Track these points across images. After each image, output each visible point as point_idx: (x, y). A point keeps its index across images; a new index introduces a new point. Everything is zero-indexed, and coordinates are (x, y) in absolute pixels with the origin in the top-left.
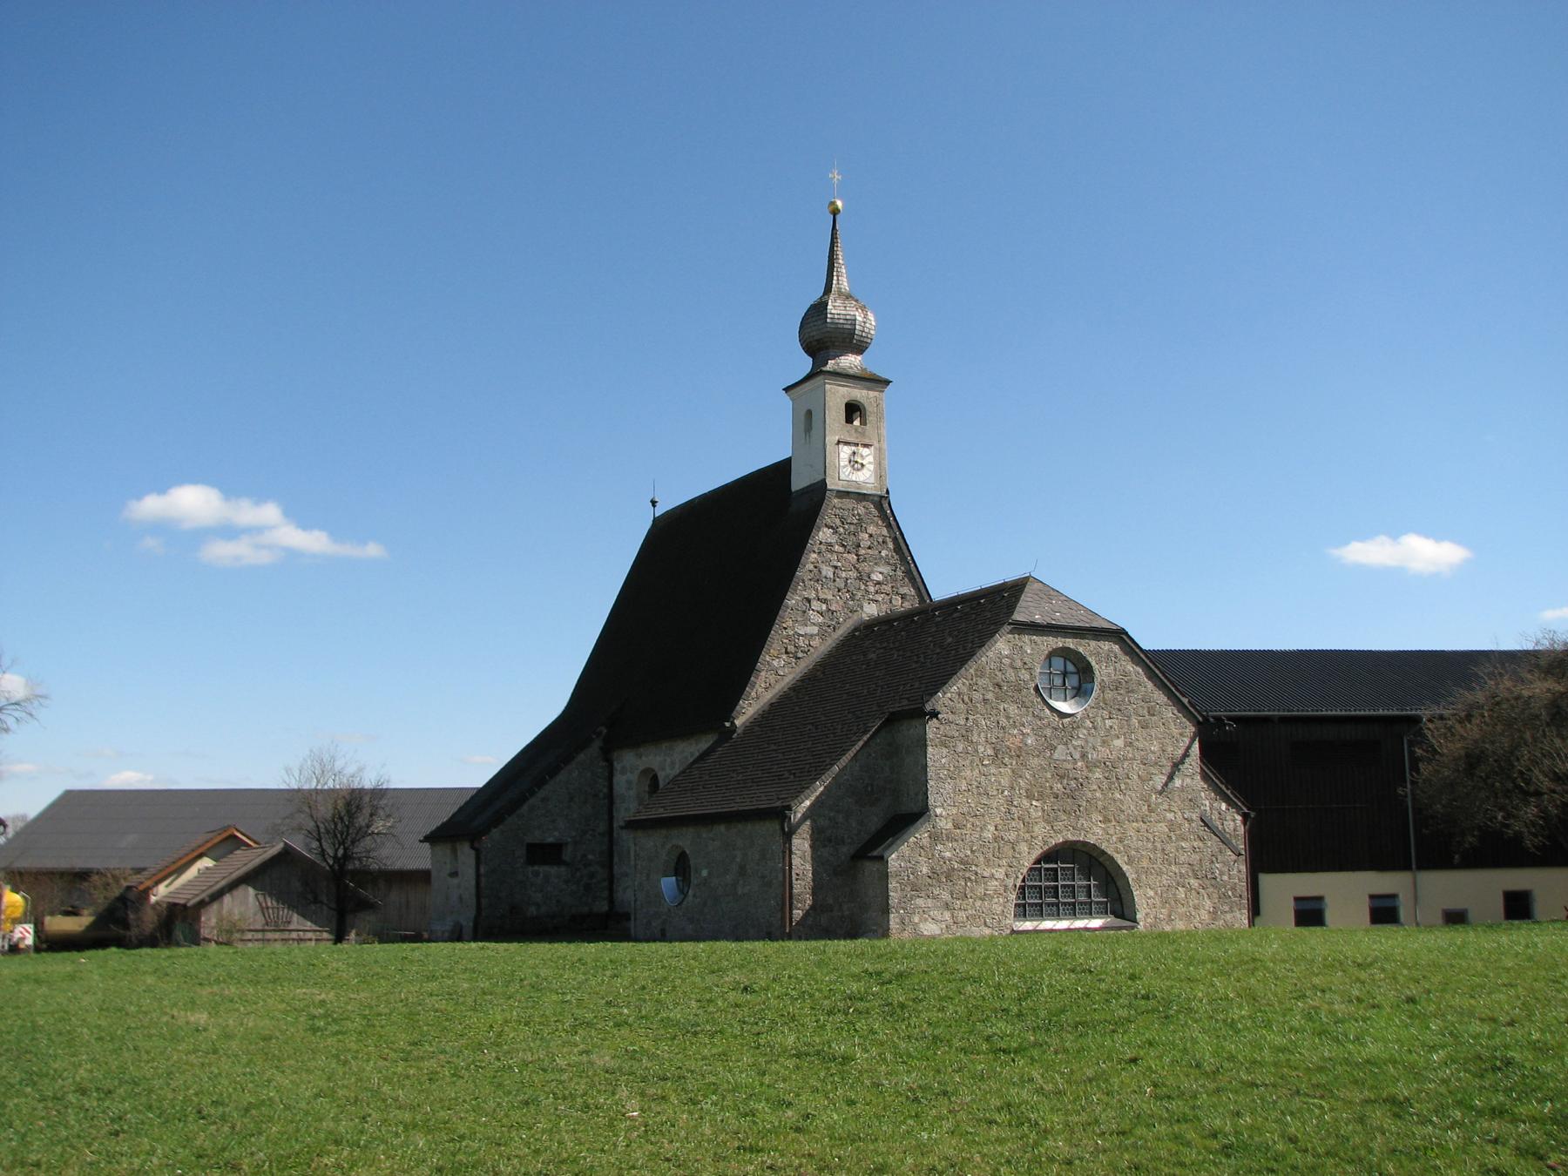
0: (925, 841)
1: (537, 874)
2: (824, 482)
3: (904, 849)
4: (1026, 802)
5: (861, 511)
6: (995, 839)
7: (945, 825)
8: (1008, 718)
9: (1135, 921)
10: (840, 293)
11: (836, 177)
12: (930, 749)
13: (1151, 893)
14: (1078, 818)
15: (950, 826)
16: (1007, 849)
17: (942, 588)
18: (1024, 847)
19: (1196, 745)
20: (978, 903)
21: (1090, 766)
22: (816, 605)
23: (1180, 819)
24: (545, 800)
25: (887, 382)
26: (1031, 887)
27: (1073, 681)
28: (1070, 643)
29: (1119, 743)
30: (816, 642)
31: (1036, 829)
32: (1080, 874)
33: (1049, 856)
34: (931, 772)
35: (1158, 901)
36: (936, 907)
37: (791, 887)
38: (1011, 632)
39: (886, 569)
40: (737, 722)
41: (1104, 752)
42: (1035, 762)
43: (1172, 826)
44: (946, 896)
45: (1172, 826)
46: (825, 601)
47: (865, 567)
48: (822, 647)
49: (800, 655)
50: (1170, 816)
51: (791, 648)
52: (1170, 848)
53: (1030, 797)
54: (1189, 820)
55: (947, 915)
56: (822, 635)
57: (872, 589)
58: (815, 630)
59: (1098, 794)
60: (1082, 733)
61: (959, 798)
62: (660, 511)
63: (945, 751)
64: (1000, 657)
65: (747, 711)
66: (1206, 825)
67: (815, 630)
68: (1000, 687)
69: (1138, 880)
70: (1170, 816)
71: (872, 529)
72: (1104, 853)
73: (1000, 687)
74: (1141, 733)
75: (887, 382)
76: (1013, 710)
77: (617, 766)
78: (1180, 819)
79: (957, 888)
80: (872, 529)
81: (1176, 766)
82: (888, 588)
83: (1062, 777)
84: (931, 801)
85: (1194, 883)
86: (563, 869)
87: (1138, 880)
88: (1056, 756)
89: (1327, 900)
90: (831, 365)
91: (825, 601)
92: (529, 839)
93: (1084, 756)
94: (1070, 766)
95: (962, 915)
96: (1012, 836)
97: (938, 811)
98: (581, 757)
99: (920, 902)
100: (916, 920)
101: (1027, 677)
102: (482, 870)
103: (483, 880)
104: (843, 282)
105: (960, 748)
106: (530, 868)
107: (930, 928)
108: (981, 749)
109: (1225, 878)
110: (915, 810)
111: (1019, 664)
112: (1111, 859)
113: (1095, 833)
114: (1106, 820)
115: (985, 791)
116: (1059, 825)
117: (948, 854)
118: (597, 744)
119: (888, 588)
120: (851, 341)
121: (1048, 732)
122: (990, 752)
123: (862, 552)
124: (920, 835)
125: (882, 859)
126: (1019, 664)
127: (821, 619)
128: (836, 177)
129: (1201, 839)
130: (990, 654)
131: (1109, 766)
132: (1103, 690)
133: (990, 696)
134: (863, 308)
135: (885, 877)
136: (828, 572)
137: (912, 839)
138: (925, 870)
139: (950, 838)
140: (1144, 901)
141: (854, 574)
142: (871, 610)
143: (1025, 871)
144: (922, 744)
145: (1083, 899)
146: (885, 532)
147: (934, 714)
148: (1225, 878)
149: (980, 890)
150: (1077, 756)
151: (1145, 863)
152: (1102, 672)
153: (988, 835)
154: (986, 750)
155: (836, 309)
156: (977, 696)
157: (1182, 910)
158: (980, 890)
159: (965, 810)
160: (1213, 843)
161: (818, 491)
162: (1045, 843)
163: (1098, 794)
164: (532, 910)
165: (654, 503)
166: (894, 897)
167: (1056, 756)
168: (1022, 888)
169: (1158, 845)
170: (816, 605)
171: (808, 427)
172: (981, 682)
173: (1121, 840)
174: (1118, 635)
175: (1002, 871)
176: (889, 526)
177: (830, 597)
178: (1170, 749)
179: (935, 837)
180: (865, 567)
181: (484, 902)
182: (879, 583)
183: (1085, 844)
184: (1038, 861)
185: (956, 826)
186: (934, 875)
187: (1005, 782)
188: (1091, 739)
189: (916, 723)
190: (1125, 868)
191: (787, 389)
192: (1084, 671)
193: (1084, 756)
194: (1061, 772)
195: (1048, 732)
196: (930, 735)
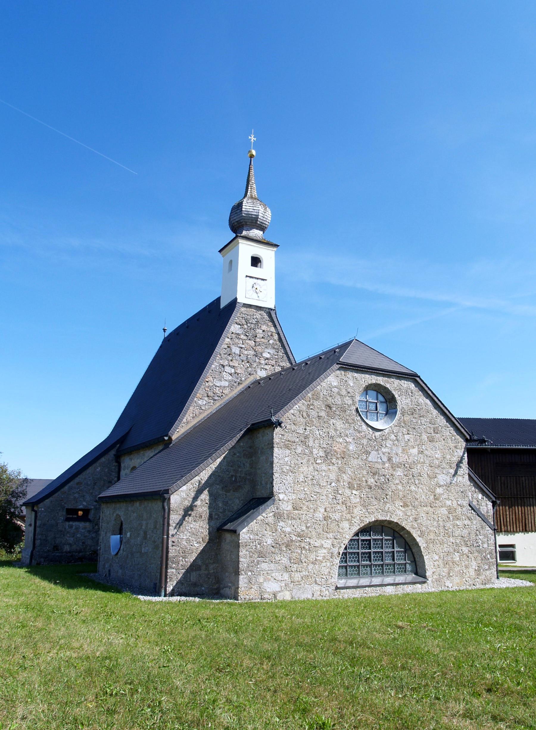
0: (271, 520)
1: (71, 527)
2: (236, 299)
3: (253, 525)
4: (348, 492)
5: (258, 316)
6: (325, 519)
7: (286, 507)
8: (336, 430)
9: (425, 577)
10: (252, 197)
11: (253, 138)
12: (276, 450)
13: (437, 557)
14: (385, 503)
15: (290, 508)
16: (333, 526)
17: (300, 357)
18: (345, 525)
19: (466, 455)
20: (311, 566)
21: (394, 467)
22: (227, 369)
23: (455, 505)
24: (78, 484)
25: (278, 246)
26: (351, 553)
27: (381, 409)
28: (380, 380)
29: (415, 451)
30: (226, 391)
31: (355, 511)
32: (385, 544)
33: (365, 530)
34: (276, 468)
35: (441, 563)
36: (278, 570)
37: (167, 552)
38: (339, 369)
39: (272, 351)
40: (174, 438)
41: (403, 458)
42: (355, 462)
43: (451, 510)
44: (285, 561)
45: (451, 510)
46: (233, 367)
47: (258, 349)
48: (231, 394)
49: (216, 398)
50: (448, 503)
51: (211, 394)
52: (448, 525)
53: (351, 487)
54: (461, 506)
55: (286, 576)
56: (231, 387)
57: (263, 362)
58: (226, 384)
59: (400, 487)
60: (389, 443)
61: (297, 487)
62: (167, 334)
63: (288, 452)
64: (331, 387)
65: (178, 432)
66: (473, 509)
67: (226, 384)
68: (330, 408)
69: (427, 547)
70: (448, 503)
71: (264, 327)
72: (403, 529)
73: (330, 408)
74: (429, 445)
75: (278, 246)
76: (339, 424)
77: (122, 465)
78: (455, 505)
79: (292, 562)
80: (264, 327)
81: (458, 466)
82: (273, 362)
83: (374, 474)
84: (276, 489)
85: (465, 550)
86: (87, 524)
87: (427, 547)
88: (370, 459)
89: (516, 546)
90: (244, 233)
91: (233, 367)
92: (70, 507)
93: (390, 459)
94: (380, 466)
95: (297, 576)
96: (337, 516)
97: (281, 496)
98: (103, 459)
99: (264, 566)
100: (261, 580)
101: (350, 402)
102: (38, 524)
103: (38, 530)
104: (253, 191)
105: (299, 450)
106: (67, 523)
107: (271, 587)
108: (315, 451)
109: (485, 546)
110: (265, 495)
111: (344, 392)
112: (409, 533)
113: (397, 514)
114: (405, 505)
115: (317, 485)
116: (372, 508)
117: (288, 529)
118: (113, 452)
119: (273, 362)
120: (254, 222)
121: (365, 441)
122: (322, 454)
123: (258, 340)
124: (266, 514)
125: (234, 532)
126: (344, 392)
127: (230, 378)
128: (253, 138)
129: (470, 519)
130: (323, 384)
131: (407, 467)
132: (403, 414)
133: (323, 414)
134: (265, 205)
135: (237, 546)
136: (235, 350)
137: (260, 518)
138: (270, 541)
139: (290, 517)
140: (431, 562)
141: (252, 352)
142: (262, 374)
143: (346, 542)
144: (271, 446)
145: (388, 561)
146: (273, 329)
147: (279, 424)
148: (485, 546)
149: (312, 557)
150: (385, 459)
151: (432, 536)
152: (402, 402)
153: (320, 515)
154: (319, 453)
155: (248, 206)
156: (313, 413)
157: (457, 569)
158: (312, 557)
159: (302, 496)
160: (477, 521)
161: (233, 304)
162: (362, 521)
163: (400, 487)
164: (67, 548)
165: (164, 330)
166: (244, 562)
167: (370, 459)
168: (345, 554)
169: (442, 524)
170: (227, 369)
171: (230, 269)
172: (316, 403)
173: (416, 520)
174: (413, 377)
175: (330, 542)
176: (275, 326)
177: (236, 365)
178: (448, 457)
179: (278, 516)
180: (258, 349)
181: (38, 542)
182: (267, 359)
183: (390, 522)
184: (357, 534)
185: (295, 509)
186: (276, 545)
187: (333, 476)
188: (394, 448)
189: (268, 431)
190: (418, 539)
191: (220, 251)
192: (390, 403)
193: (390, 459)
194: (374, 470)
195: (365, 441)
196: (276, 440)
